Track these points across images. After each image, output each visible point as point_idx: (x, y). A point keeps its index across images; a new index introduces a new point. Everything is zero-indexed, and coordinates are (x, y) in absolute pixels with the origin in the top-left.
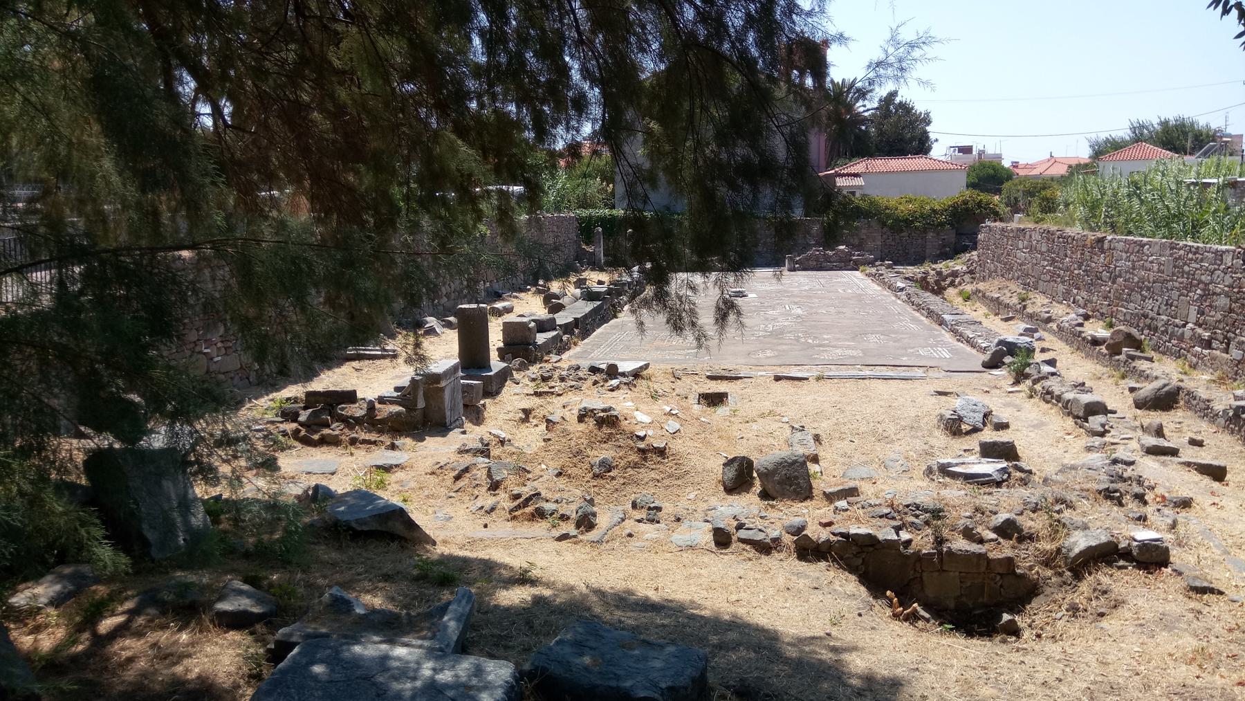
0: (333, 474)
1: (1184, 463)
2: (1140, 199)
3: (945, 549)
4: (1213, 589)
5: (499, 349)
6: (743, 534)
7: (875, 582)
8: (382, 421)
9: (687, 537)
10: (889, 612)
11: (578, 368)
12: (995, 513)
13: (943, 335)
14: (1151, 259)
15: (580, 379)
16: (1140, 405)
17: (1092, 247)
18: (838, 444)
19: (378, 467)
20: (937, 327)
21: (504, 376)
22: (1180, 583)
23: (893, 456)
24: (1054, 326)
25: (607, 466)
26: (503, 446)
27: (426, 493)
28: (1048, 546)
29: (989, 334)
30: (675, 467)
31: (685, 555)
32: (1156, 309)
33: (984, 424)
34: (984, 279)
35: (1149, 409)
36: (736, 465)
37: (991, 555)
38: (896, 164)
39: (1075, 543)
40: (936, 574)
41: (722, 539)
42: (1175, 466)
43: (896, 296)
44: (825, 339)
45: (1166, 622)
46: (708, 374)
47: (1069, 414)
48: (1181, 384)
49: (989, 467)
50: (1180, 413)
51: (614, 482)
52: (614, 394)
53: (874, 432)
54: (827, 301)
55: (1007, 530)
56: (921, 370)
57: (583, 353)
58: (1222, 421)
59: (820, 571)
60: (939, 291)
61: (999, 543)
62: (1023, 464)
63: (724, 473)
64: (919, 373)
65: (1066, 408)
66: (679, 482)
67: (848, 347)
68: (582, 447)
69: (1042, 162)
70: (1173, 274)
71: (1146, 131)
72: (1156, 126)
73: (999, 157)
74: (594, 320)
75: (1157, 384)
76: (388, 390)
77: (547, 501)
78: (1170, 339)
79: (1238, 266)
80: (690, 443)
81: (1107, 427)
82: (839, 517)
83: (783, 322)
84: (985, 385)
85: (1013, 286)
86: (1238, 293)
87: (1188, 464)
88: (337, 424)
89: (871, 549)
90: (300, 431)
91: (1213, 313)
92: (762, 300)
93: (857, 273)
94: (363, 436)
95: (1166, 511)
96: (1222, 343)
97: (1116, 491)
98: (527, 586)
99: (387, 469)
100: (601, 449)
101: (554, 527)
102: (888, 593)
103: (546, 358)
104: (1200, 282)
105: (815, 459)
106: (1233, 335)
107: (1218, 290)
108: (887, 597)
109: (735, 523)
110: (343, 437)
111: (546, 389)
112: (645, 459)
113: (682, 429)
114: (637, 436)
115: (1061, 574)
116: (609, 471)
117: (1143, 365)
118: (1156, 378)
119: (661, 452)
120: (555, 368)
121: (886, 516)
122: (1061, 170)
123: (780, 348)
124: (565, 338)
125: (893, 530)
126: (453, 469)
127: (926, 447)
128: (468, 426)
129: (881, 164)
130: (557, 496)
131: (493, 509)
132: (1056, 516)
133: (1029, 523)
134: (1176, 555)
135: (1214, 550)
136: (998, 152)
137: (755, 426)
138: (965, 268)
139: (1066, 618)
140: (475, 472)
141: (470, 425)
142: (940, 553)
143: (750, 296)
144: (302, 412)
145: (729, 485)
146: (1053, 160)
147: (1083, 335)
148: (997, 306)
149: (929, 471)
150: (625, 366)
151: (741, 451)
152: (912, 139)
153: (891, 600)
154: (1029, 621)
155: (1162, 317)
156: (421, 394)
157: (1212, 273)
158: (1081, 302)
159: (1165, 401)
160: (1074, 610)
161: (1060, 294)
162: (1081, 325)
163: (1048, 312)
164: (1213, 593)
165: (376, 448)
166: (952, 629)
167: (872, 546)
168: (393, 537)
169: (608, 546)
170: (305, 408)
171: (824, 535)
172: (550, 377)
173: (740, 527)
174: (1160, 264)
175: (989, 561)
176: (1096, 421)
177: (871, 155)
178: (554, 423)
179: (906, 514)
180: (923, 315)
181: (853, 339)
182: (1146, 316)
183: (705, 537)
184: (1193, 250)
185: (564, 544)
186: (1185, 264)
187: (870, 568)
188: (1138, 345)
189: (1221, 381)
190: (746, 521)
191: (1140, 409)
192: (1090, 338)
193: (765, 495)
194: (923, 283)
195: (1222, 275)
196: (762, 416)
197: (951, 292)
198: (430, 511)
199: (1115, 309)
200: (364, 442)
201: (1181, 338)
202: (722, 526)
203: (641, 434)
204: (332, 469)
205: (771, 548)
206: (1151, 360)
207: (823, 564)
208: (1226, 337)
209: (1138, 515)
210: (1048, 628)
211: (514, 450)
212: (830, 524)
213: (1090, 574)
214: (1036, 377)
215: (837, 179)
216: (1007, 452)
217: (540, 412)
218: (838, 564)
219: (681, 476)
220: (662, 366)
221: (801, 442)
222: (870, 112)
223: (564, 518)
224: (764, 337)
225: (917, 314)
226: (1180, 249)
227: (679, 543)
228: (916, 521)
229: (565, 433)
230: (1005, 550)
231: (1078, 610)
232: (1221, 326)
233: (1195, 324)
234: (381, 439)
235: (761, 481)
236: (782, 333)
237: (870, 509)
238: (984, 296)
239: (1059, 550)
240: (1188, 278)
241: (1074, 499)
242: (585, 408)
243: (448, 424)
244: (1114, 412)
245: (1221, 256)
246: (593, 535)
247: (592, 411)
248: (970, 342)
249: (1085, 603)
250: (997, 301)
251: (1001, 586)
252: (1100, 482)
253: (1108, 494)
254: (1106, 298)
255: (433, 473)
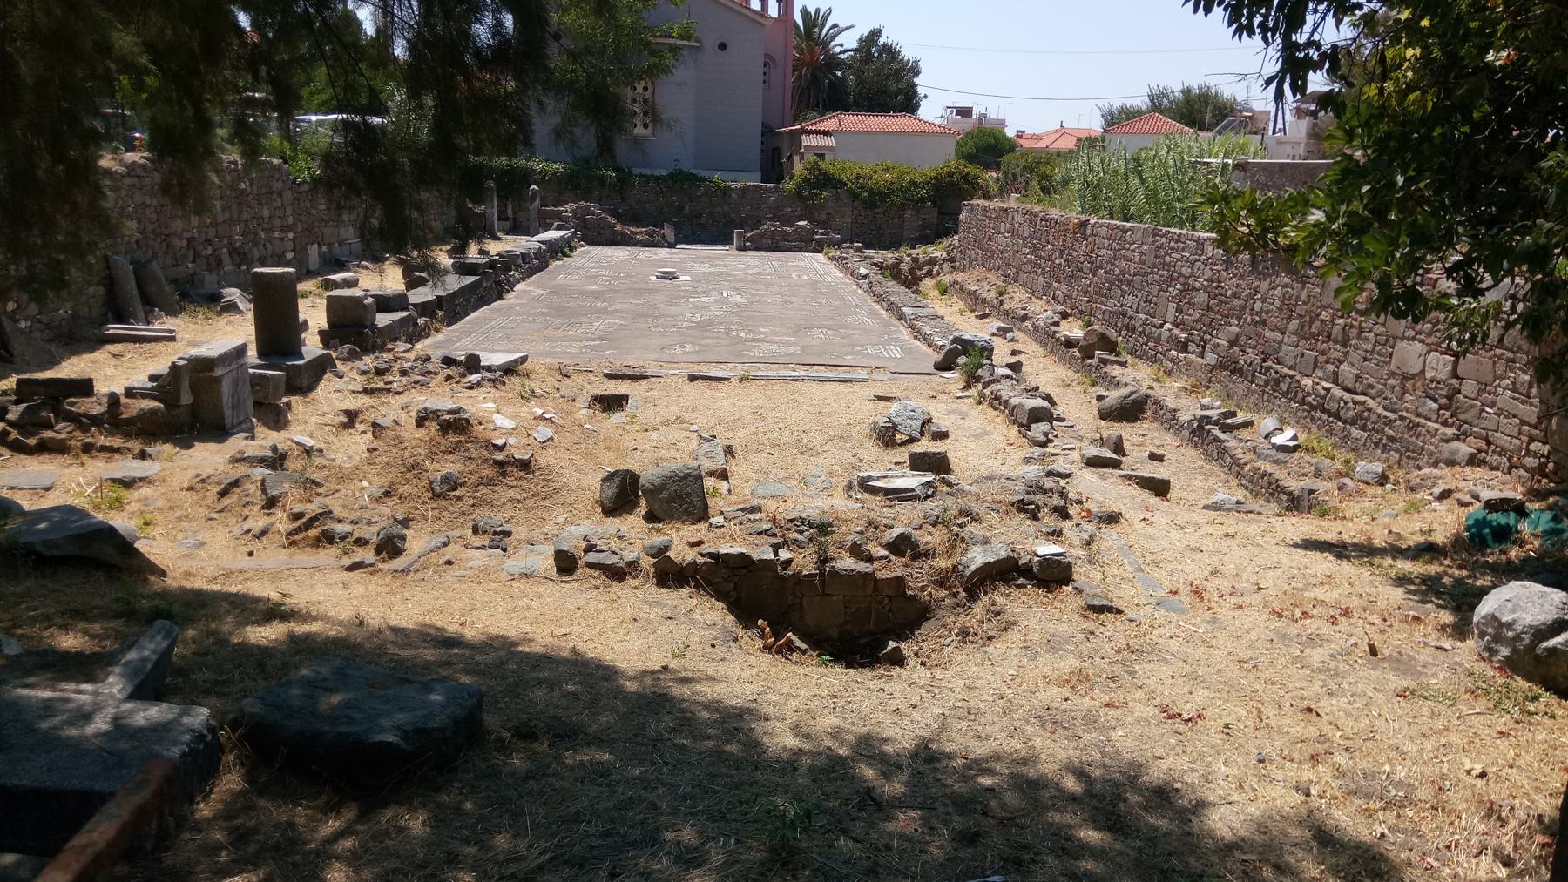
0: (48, 489)
1: (1124, 476)
2: (1141, 178)
3: (828, 569)
4: (1112, 607)
5: (321, 333)
6: (592, 557)
7: (745, 612)
8: (130, 421)
9: (522, 564)
10: (759, 643)
11: (428, 359)
12: (891, 528)
13: (901, 332)
14: (1133, 247)
15: (429, 373)
16: (1105, 415)
17: (1075, 233)
18: (752, 457)
19: (114, 481)
20: (897, 322)
21: (321, 367)
22: (1079, 602)
23: (815, 471)
24: (1028, 324)
25: (451, 483)
26: (309, 456)
27: (178, 514)
28: (942, 563)
29: (950, 328)
30: (542, 484)
31: (515, 584)
32: (1135, 307)
33: (922, 434)
34: (964, 269)
35: (1113, 420)
36: (617, 480)
37: (879, 575)
38: (875, 122)
39: (972, 560)
40: (817, 599)
41: (566, 564)
42: (1114, 479)
43: (858, 285)
44: (761, 333)
45: (1053, 645)
46: (606, 371)
47: (1015, 422)
48: (1150, 391)
49: (913, 481)
50: (1146, 425)
51: (461, 503)
52: (472, 393)
53: (797, 443)
54: (776, 289)
55: (902, 546)
56: (866, 370)
57: (436, 344)
58: (1186, 433)
59: (682, 598)
60: (912, 282)
61: (889, 561)
62: (951, 478)
63: (602, 489)
64: (862, 374)
65: (1011, 415)
66: (547, 503)
67: (787, 343)
68: (419, 459)
69: (1048, 134)
70: (1154, 267)
71: (1165, 101)
72: (1177, 94)
73: (1002, 124)
74: (468, 300)
75: (1123, 392)
76: (140, 380)
77: (340, 521)
78: (1147, 341)
79: (1219, 257)
80: (565, 455)
81: (1050, 436)
82: (711, 535)
83: (715, 311)
84: (933, 389)
85: (993, 277)
86: (1216, 288)
87: (1129, 477)
88: (63, 424)
89: (744, 571)
90: (9, 433)
91: (1191, 311)
92: (696, 285)
93: (820, 257)
94: (102, 440)
95: (1085, 526)
96: (1198, 346)
97: (1031, 503)
98: (275, 623)
99: (128, 484)
100: (446, 461)
101: (345, 553)
102: (760, 621)
103: (390, 346)
104: (1181, 275)
105: (723, 475)
106: (1209, 337)
107: (1197, 285)
108: (758, 627)
109: (584, 545)
110: (73, 443)
111: (381, 385)
112: (503, 474)
113: (556, 437)
114: (494, 445)
115: (955, 595)
116: (455, 489)
117: (1115, 371)
118: (1126, 385)
119: (525, 465)
120: (396, 359)
121: (765, 532)
122: (1068, 143)
123: (703, 342)
124: (421, 321)
125: (771, 549)
126: (218, 483)
127: (854, 460)
128: (261, 430)
129: (852, 121)
130: (354, 516)
131: (264, 533)
132: (956, 529)
133: (925, 538)
134: (1081, 574)
135: (1127, 568)
136: (1001, 117)
137: (654, 436)
138: (944, 255)
139: (955, 644)
140: (248, 485)
141: (264, 429)
142: (822, 574)
143: (682, 278)
144: (12, 407)
145: (608, 504)
146: (1063, 131)
147: (1057, 335)
148: (974, 302)
149: (850, 486)
150: (487, 359)
151: (632, 464)
152: (899, 92)
153: (763, 630)
154: (915, 648)
155: (1141, 315)
156: (186, 384)
157: (1193, 264)
158: (1061, 298)
159: (1131, 410)
160: (964, 634)
161: (1040, 288)
162: (1056, 324)
163: (1024, 309)
164: (1111, 612)
165: (120, 457)
166: (830, 661)
167: (745, 567)
168: (98, 564)
169: (416, 576)
170: (17, 402)
171: (690, 555)
172: (387, 370)
173: (590, 548)
174: (1142, 254)
175: (876, 581)
176: (1038, 430)
177: (846, 109)
178: (383, 428)
179: (789, 529)
180: (883, 307)
181: (795, 333)
182: (1124, 315)
183: (543, 560)
184: (1176, 237)
185: (356, 575)
186: (1166, 254)
187: (743, 594)
188: (1112, 347)
189: (1193, 390)
190: (599, 543)
191: (1104, 420)
192: (1063, 339)
193: (651, 517)
194: (895, 272)
195: (1203, 267)
196: (667, 423)
197: (927, 283)
198: (180, 536)
199: (1094, 305)
200: (104, 449)
201: (1158, 341)
202: (566, 548)
203: (500, 442)
204: (48, 483)
205: (625, 574)
206: (1124, 365)
207: (686, 591)
208: (1202, 339)
209: (1052, 529)
210: (934, 656)
211: (325, 462)
212: (699, 543)
213: (985, 593)
214: (987, 379)
215: (804, 137)
216: (937, 464)
217: (371, 416)
218: (704, 590)
219: (550, 494)
220: (548, 361)
221: (709, 455)
222: (847, 54)
223: (361, 542)
224: (687, 328)
225: (877, 307)
226: (1162, 236)
227: (511, 571)
228: (800, 537)
229: (398, 441)
230: (897, 568)
231: (968, 634)
232: (1198, 327)
233: (1173, 324)
234: (128, 445)
235: (646, 500)
236: (711, 324)
237: (748, 525)
238: (961, 289)
239: (955, 567)
240: (1168, 271)
241: (982, 512)
242: (426, 409)
243: (228, 426)
244: (1063, 420)
245: (1203, 244)
246: (399, 563)
247: (435, 412)
248: (927, 340)
249: (976, 627)
250: (973, 295)
251: (890, 611)
252: (1014, 492)
253: (1022, 507)
254: (1086, 293)
255: (191, 489)
